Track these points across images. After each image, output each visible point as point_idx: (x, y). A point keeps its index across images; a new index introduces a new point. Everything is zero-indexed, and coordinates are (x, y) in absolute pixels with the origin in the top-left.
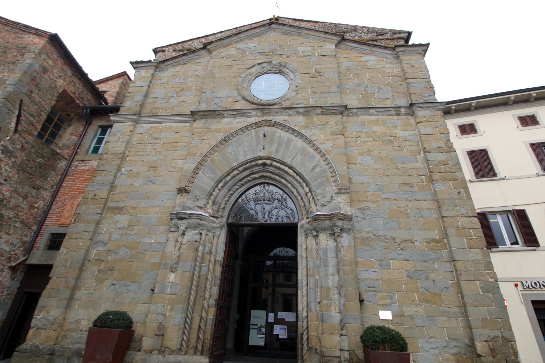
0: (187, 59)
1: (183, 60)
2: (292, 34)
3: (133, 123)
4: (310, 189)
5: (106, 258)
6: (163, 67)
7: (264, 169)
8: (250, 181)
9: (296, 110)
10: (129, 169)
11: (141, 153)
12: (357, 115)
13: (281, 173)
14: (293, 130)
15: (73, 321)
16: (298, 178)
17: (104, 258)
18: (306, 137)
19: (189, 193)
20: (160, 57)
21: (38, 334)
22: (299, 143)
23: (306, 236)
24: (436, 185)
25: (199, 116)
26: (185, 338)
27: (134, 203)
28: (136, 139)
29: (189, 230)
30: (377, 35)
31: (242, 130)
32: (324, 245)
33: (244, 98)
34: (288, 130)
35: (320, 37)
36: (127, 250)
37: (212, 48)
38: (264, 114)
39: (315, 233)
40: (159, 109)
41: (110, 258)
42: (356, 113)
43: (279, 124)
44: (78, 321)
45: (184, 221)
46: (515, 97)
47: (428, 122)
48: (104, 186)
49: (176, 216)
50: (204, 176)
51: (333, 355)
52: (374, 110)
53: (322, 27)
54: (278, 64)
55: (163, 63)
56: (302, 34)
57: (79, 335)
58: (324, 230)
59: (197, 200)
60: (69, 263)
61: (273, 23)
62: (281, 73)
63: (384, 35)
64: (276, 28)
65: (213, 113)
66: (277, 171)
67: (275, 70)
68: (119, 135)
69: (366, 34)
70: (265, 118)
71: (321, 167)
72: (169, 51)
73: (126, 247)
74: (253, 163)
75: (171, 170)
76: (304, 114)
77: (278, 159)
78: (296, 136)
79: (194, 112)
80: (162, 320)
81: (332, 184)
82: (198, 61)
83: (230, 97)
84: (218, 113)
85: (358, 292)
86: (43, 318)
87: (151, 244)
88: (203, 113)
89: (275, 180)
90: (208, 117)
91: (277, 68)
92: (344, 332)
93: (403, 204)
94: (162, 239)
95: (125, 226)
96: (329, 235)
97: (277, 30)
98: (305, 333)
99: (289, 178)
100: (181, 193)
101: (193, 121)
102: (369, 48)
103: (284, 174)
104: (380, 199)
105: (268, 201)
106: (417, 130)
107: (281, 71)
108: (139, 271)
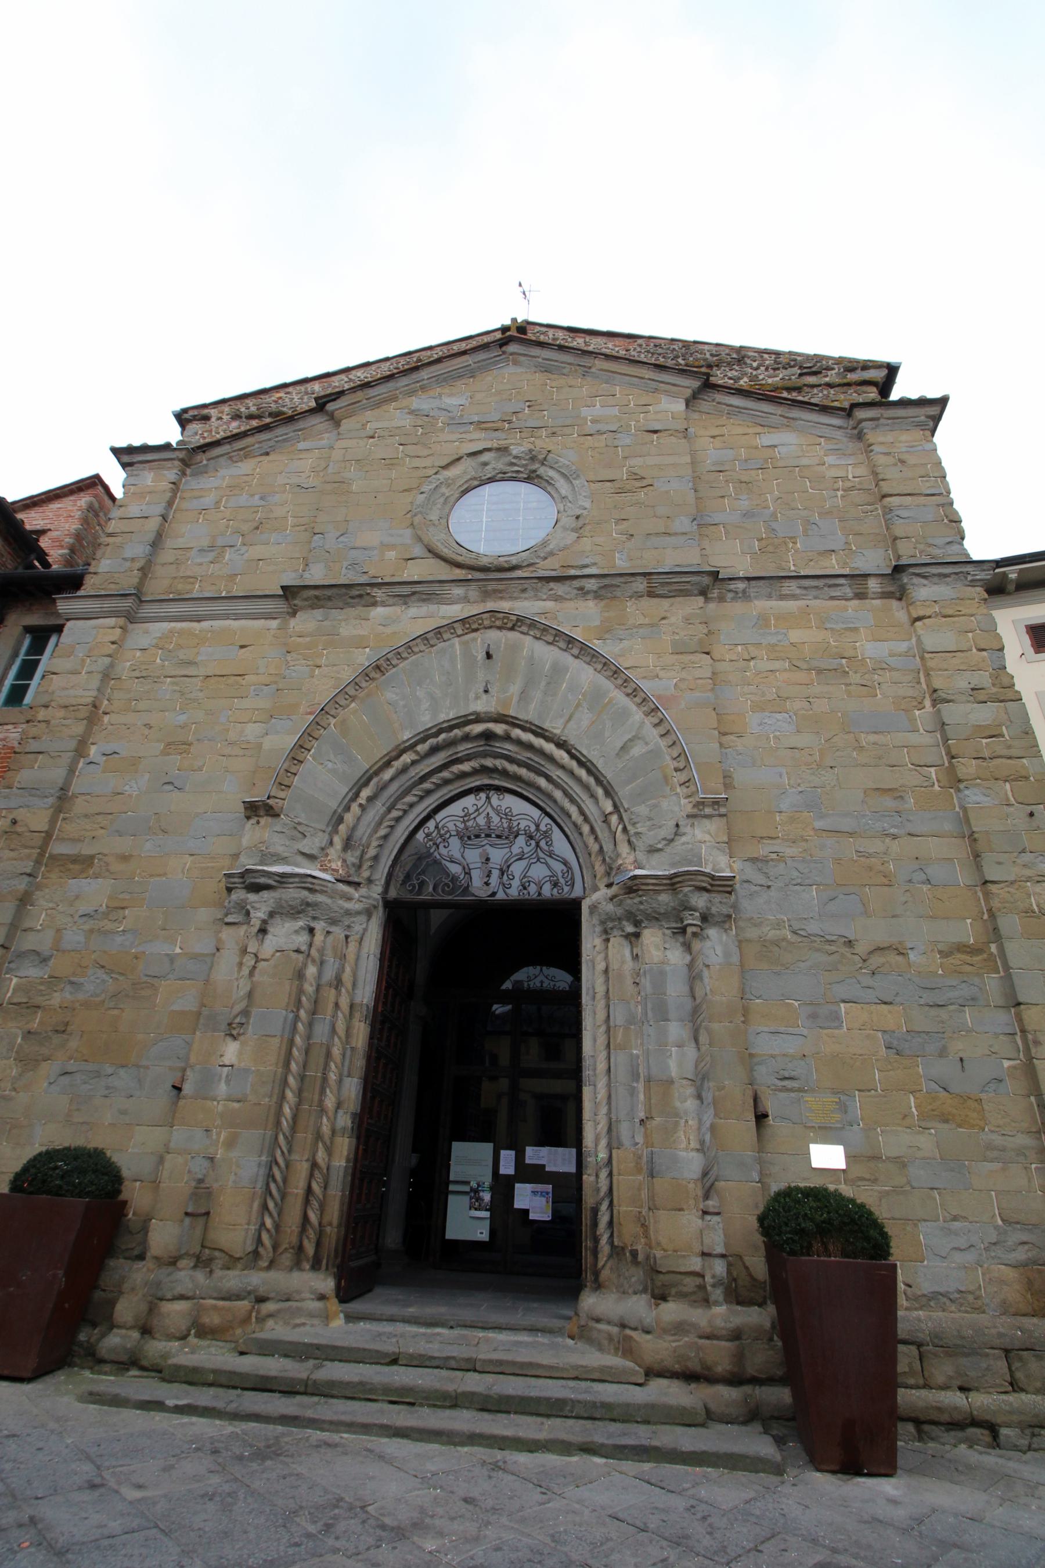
0: (270, 440)
1: (260, 442)
2: (565, 371)
4: (615, 806)
5: (47, 997)
6: (205, 462)
7: (488, 748)
8: (447, 782)
9: (576, 583)
13: (536, 759)
16: (582, 773)
18: (604, 660)
20: (196, 434)
23: (604, 937)
25: (306, 600)
26: (269, 1222)
28: (129, 664)
29: (278, 920)
30: (801, 375)
31: (427, 639)
33: (430, 551)
37: (340, 408)
38: (486, 595)
39: (630, 929)
40: (192, 580)
41: (56, 999)
42: (744, 591)
43: (528, 622)
45: (265, 894)
47: (945, 617)
48: (39, 796)
50: (320, 767)
51: (682, 1269)
52: (794, 584)
53: (648, 352)
56: (593, 370)
58: (655, 918)
59: (300, 836)
61: (510, 341)
66: (524, 755)
67: (518, 472)
68: (81, 655)
69: (772, 372)
70: (491, 605)
72: (220, 418)
73: (103, 967)
74: (457, 732)
75: (228, 751)
76: (597, 595)
77: (527, 722)
78: (577, 657)
81: (678, 790)
83: (392, 547)
84: (358, 593)
85: (750, 1093)
87: (172, 959)
88: (316, 593)
89: (518, 778)
90: (330, 604)
91: (523, 466)
92: (712, 1204)
93: (876, 846)
94: (203, 945)
96: (668, 932)
97: (522, 359)
98: (604, 1207)
99: (556, 773)
102: (779, 410)
103: (543, 763)
104: (812, 833)
106: (914, 640)
107: (534, 475)
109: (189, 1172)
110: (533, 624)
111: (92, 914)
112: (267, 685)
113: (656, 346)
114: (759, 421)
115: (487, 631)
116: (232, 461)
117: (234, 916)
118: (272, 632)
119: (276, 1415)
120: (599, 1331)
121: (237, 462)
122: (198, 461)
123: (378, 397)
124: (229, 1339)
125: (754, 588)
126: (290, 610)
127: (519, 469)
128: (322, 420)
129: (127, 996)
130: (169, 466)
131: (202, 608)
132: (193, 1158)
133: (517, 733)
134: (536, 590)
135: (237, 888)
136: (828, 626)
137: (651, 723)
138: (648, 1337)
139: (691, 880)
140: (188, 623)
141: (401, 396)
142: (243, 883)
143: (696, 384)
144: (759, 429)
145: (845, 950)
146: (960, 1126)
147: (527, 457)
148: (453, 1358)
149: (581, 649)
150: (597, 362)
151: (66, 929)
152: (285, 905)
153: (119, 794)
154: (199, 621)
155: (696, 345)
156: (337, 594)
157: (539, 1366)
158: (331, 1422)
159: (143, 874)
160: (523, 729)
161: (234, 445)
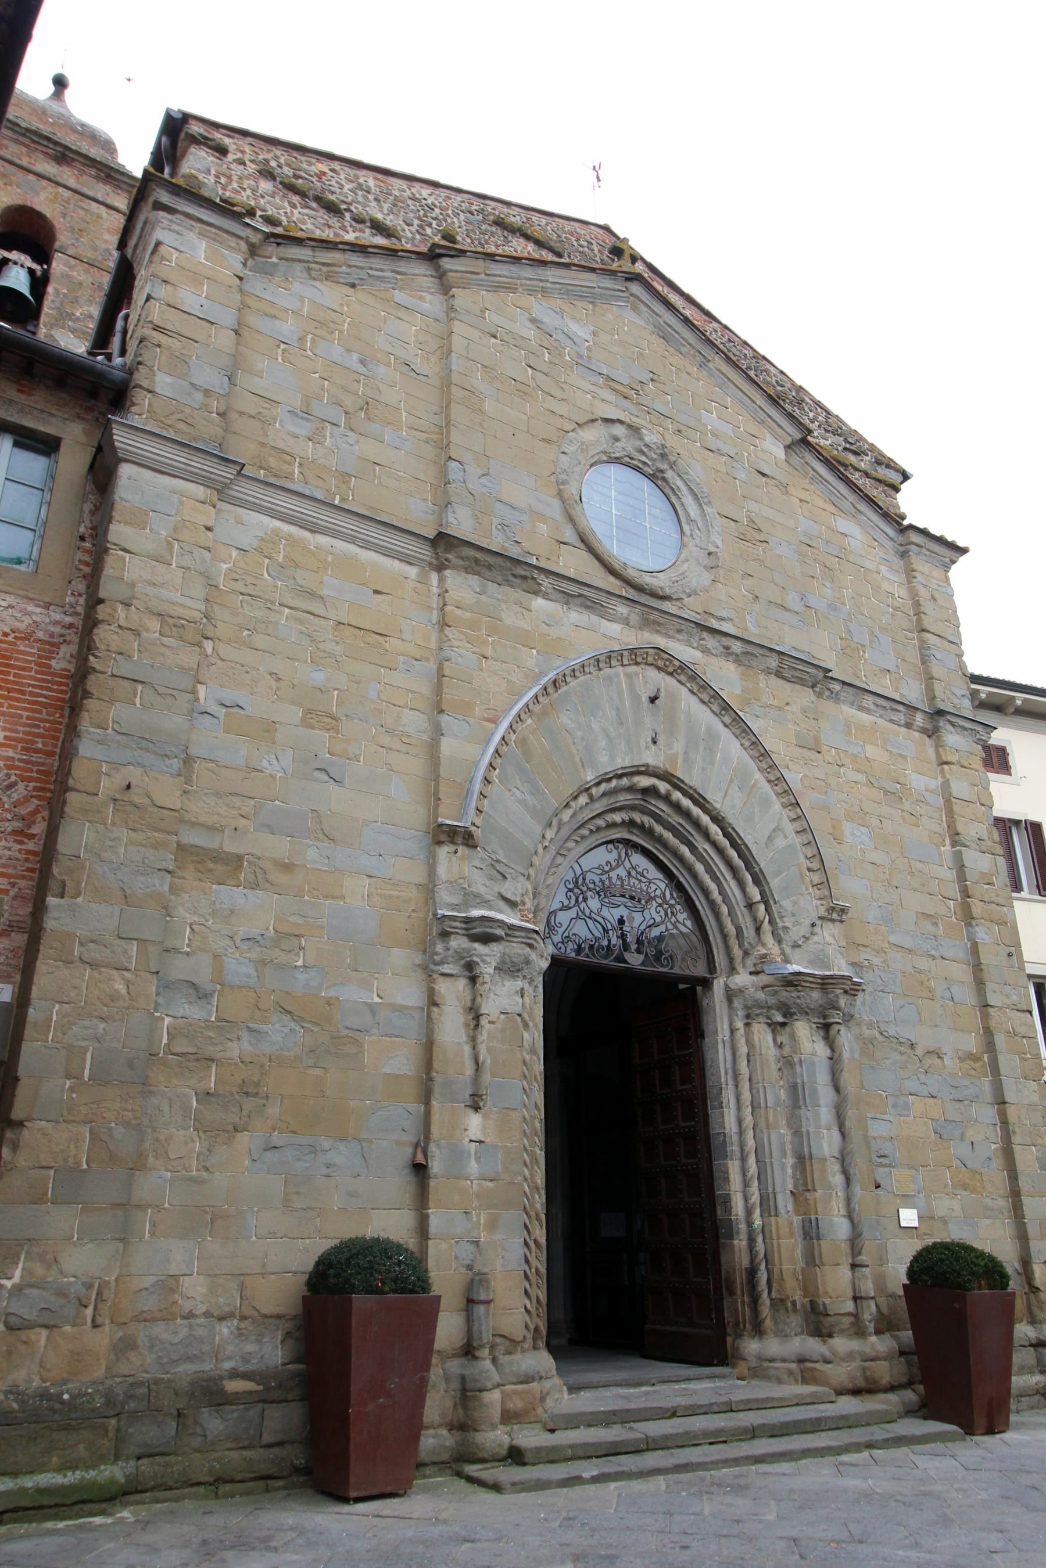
0: (362, 268)
1: (350, 266)
2: (683, 349)
3: (209, 491)
5: (220, 1048)
6: (274, 260)
7: (642, 803)
9: (726, 641)
10: (230, 695)
11: (259, 641)
12: (835, 697)
13: (688, 827)
14: (724, 704)
15: (147, 1285)
16: (733, 853)
17: (211, 1048)
18: (754, 739)
19: (476, 847)
21: (22, 1348)
22: (732, 746)
24: (977, 929)
25: (462, 558)
27: (279, 847)
28: (225, 566)
30: (845, 449)
32: (808, 1051)
33: (583, 541)
34: (709, 701)
35: (754, 402)
36: (293, 1024)
37: (457, 271)
40: (288, 458)
41: (234, 1050)
43: (690, 673)
44: (169, 1285)
46: (989, 694)
47: (962, 766)
48: (155, 753)
49: (463, 926)
50: (507, 794)
51: (843, 1311)
52: (871, 698)
54: (658, 448)
55: (278, 244)
56: (710, 365)
57: (185, 1331)
58: (805, 1012)
59: (499, 877)
60: (88, 1066)
61: (636, 279)
62: (657, 478)
63: (859, 454)
64: (642, 302)
65: (508, 564)
66: (675, 819)
67: (645, 463)
68: (163, 533)
71: (786, 837)
73: (289, 1012)
75: (386, 740)
76: (738, 661)
77: (691, 787)
78: (726, 725)
79: (452, 539)
80: (471, 1256)
82: (399, 296)
83: (543, 518)
84: (523, 573)
86: (33, 1286)
87: (372, 1008)
88: (478, 555)
89: (660, 840)
90: (487, 573)
91: (652, 459)
93: (923, 964)
95: (267, 934)
96: (814, 1026)
97: (643, 308)
99: (703, 845)
100: (453, 842)
101: (430, 564)
102: (852, 497)
103: (693, 833)
104: (887, 945)
105: (632, 898)
107: (659, 475)
108: (352, 1103)
109: (456, 1258)
110: (694, 677)
111: (259, 938)
112: (417, 660)
113: (730, 341)
114: (834, 498)
115: (647, 667)
116: (310, 275)
117: (451, 966)
118: (412, 584)
119: (671, 1466)
120: (777, 1368)
121: (314, 279)
122: (267, 254)
123: (498, 279)
124: (533, 1420)
125: (847, 693)
126: (435, 562)
127: (646, 460)
128: (429, 273)
129: (328, 1052)
130: (233, 245)
131: (325, 517)
132: (457, 1242)
133: (677, 795)
134: (691, 635)
135: (457, 933)
136: (889, 748)
137: (788, 816)
138: (830, 1366)
139: (843, 984)
140: (297, 528)
141: (520, 289)
142: (467, 929)
143: (798, 436)
144: (833, 509)
145: (909, 1051)
146: (972, 1193)
147: (658, 451)
148: (715, 1403)
149: (734, 720)
150: (717, 358)
151: (226, 955)
152: (508, 961)
153: (257, 770)
154: (312, 531)
155: (764, 362)
156: (500, 566)
157: (773, 1399)
158: (712, 1463)
159: (315, 893)
160: (685, 793)
161: (318, 254)
